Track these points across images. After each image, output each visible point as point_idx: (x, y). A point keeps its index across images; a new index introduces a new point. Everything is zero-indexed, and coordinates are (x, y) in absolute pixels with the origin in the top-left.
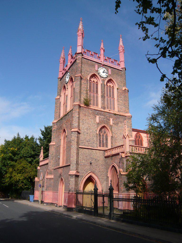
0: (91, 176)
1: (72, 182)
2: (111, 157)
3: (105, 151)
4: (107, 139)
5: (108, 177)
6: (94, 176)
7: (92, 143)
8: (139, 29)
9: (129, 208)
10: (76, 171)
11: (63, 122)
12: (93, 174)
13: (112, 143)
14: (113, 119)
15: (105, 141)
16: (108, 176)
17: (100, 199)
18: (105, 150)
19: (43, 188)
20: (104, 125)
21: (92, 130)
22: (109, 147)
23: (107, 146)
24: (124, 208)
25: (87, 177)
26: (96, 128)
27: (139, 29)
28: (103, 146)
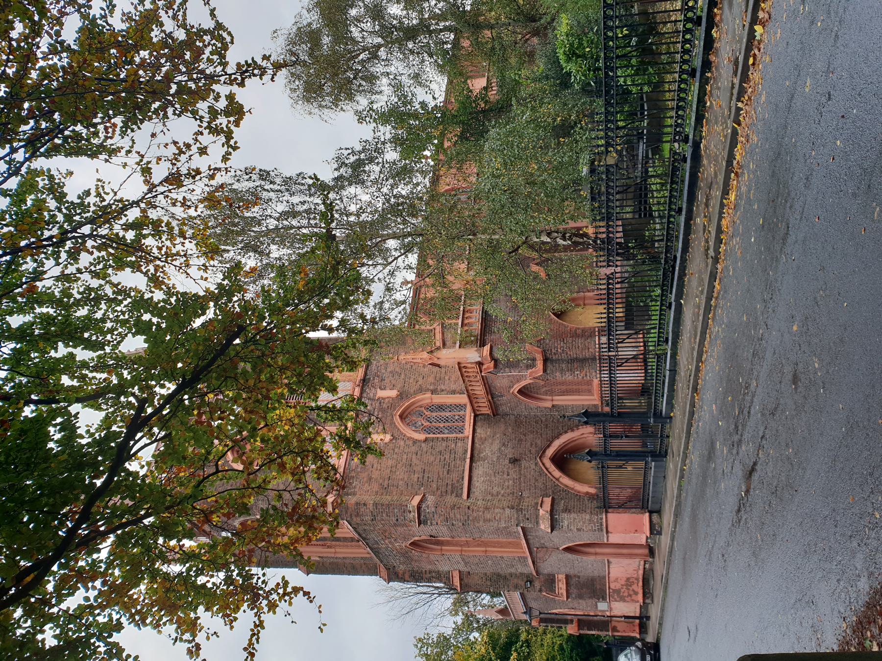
0: (553, 459)
1: (574, 521)
2: (492, 398)
3: (476, 416)
4: (441, 407)
5: (553, 406)
6: (550, 452)
7: (452, 456)
8: (253, 59)
9: (640, 342)
10: (539, 508)
11: (387, 548)
12: (547, 451)
13: (453, 392)
14: (382, 389)
15: (448, 414)
16: (550, 406)
17: (617, 444)
18: (473, 414)
19: (606, 518)
20: (398, 417)
21: (414, 456)
22: (463, 399)
23: (462, 407)
24: (640, 368)
25: (557, 473)
26: (408, 442)
27: (253, 59)
28: (462, 419)
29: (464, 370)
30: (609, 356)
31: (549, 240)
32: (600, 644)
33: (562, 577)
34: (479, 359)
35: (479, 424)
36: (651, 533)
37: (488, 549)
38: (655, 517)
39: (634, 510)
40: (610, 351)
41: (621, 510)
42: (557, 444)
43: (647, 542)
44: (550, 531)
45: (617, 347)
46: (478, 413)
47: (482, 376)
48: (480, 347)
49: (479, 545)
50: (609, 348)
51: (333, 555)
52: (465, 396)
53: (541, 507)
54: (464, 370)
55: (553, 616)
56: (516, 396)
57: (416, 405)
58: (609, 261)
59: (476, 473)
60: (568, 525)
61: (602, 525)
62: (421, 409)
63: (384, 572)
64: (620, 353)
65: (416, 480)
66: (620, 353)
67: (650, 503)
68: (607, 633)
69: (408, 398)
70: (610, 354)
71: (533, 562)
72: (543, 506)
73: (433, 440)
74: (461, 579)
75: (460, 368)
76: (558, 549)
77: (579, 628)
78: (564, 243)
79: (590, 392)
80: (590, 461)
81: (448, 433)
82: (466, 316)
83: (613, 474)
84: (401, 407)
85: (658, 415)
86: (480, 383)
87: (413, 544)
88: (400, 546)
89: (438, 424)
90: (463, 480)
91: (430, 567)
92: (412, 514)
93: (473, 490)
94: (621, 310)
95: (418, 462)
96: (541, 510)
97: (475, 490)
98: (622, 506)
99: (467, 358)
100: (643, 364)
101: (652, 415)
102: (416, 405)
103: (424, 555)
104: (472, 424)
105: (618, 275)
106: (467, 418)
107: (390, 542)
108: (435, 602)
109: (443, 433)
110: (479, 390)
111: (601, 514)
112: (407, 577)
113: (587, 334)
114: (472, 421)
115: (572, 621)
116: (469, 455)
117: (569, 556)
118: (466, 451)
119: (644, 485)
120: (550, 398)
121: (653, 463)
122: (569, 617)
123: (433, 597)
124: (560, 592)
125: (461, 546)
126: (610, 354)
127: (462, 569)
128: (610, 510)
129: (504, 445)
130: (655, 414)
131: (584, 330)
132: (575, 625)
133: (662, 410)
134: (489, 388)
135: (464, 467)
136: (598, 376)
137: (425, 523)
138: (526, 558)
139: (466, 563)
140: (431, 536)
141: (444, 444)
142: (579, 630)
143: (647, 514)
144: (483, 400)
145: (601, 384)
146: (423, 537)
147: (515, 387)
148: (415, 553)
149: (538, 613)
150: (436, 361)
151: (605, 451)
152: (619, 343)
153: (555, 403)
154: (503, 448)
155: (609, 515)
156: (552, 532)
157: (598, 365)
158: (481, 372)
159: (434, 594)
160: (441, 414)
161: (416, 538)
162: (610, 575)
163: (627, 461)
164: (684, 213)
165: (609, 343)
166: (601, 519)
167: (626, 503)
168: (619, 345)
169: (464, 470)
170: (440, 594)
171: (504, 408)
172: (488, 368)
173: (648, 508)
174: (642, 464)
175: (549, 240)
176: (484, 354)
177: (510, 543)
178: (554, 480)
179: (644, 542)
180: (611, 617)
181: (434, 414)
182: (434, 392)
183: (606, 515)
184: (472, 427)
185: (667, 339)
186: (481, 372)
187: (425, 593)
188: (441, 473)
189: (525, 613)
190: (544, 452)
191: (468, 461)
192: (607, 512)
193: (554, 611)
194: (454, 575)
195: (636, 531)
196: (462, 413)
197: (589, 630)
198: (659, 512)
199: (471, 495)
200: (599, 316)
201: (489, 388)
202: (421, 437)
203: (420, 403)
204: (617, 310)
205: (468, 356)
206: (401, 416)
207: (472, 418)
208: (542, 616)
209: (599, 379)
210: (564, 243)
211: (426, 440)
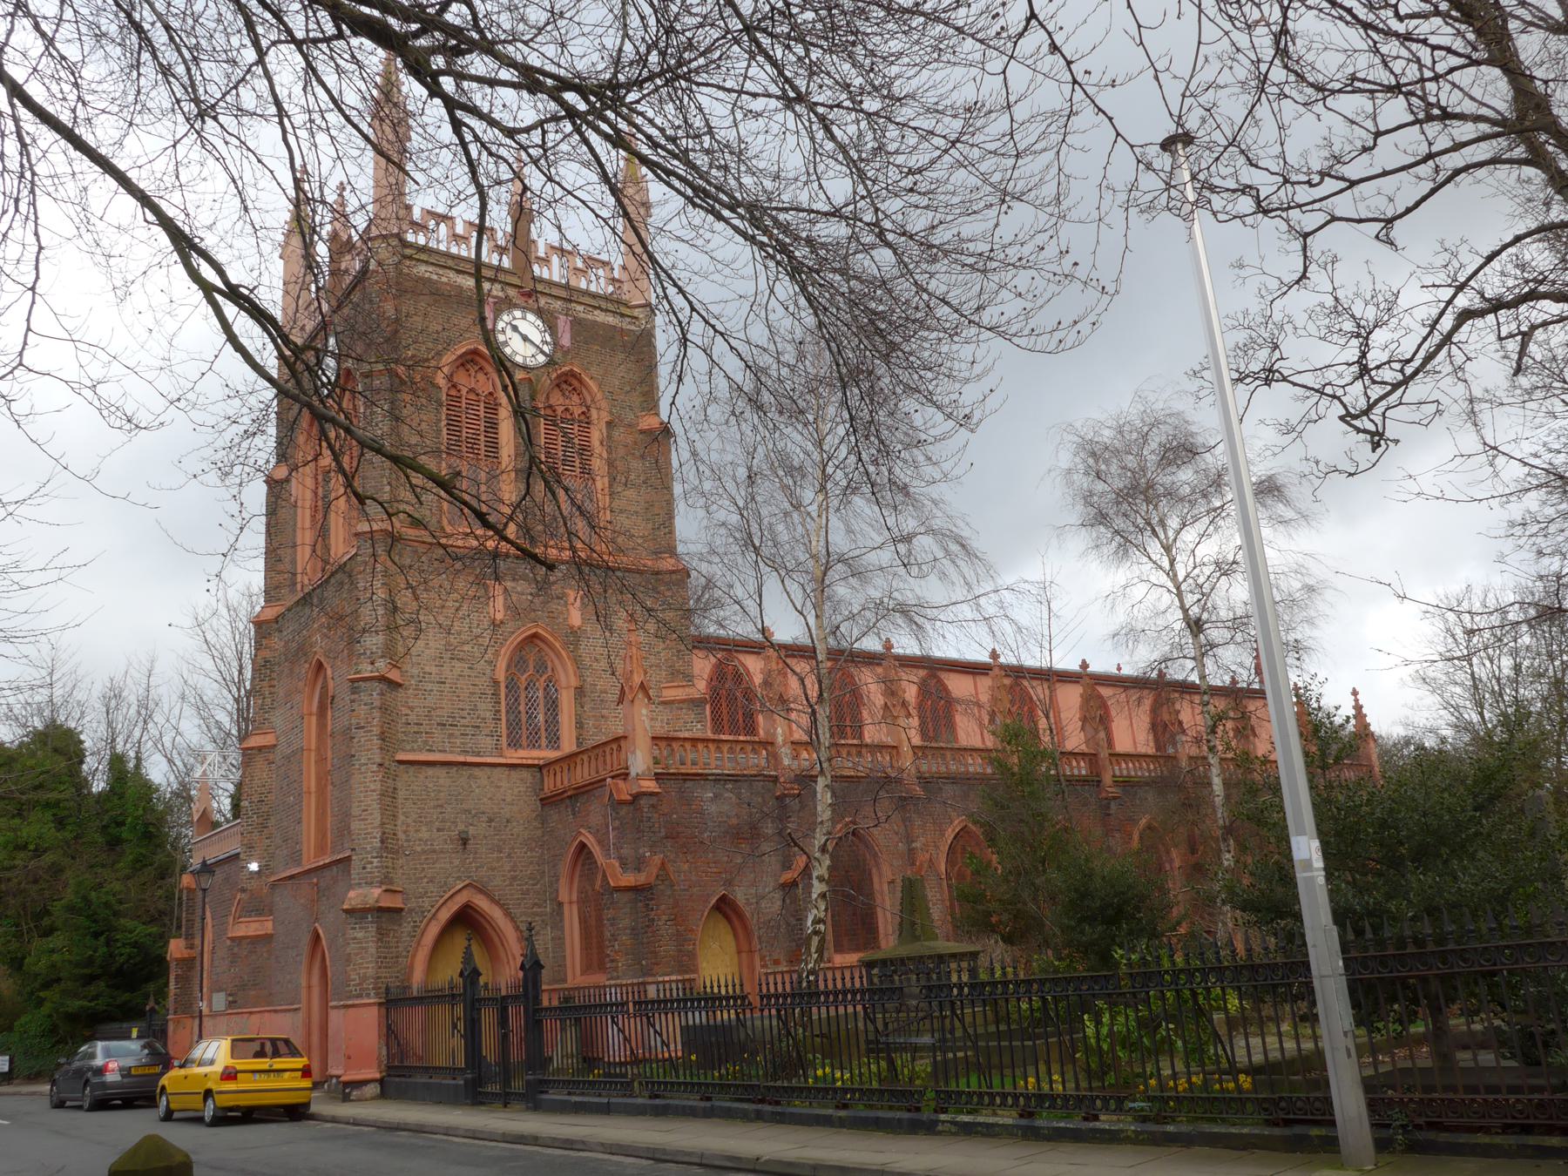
3: (540, 768)
6: (482, 903)
10: (384, 887)
12: (482, 896)
13: (580, 725)
18: (541, 762)
19: (369, 1004)
20: (534, 631)
22: (568, 745)
23: (554, 741)
28: (534, 744)
29: (615, 746)
30: (627, 1003)
31: (814, 896)
32: (152, 998)
33: (268, 927)
34: (633, 773)
35: (525, 774)
36: (347, 1084)
37: (313, 796)
38: (372, 1089)
39: (384, 1052)
40: (635, 1003)
41: (385, 1030)
42: (496, 914)
43: (332, 1077)
44: (345, 907)
45: (641, 1016)
46: (545, 771)
47: (605, 780)
48: (656, 774)
49: (319, 779)
50: (640, 1003)
51: (299, 525)
52: (574, 748)
53: (386, 891)
54: (615, 746)
55: (199, 912)
56: (575, 838)
57: (556, 661)
58: (769, 997)
59: (441, 772)
60: (355, 938)
61: (360, 996)
62: (549, 669)
63: (271, 613)
64: (632, 1020)
65: (427, 669)
66: (632, 1020)
67: (397, 1079)
68: (171, 1012)
69: (566, 644)
70: (631, 1005)
71: (291, 877)
72: (388, 894)
73: (496, 694)
74: (260, 749)
75: (617, 740)
76: (317, 920)
77: (180, 961)
78: (809, 923)
79: (587, 969)
80: (461, 974)
81: (507, 721)
82: (710, 745)
83: (443, 1015)
84: (552, 636)
85: (542, 1085)
86: (594, 776)
87: (320, 666)
88: (316, 642)
89: (522, 700)
90: (429, 750)
91: (281, 694)
92: (370, 668)
93: (412, 769)
94: (697, 1021)
95: (457, 671)
96: (379, 890)
97: (411, 773)
98: (390, 1033)
99: (634, 752)
100: (648, 1066)
101: (540, 1077)
102: (556, 661)
103: (301, 684)
104: (524, 762)
105: (748, 1015)
106: (536, 753)
107: (322, 626)
108: (225, 692)
109: (507, 712)
110: (583, 774)
111: (377, 994)
112: (263, 654)
113: (686, 962)
114: (530, 762)
115: (191, 947)
116: (470, 759)
117: (306, 940)
118: (478, 754)
119: (427, 1069)
120: (575, 897)
121: (462, 1082)
122: (197, 941)
123: (234, 690)
124: (243, 925)
125: (318, 749)
126: (631, 1005)
127: (278, 750)
128: (383, 1011)
129: (491, 820)
130: (541, 1082)
131: (692, 956)
132: (186, 953)
133: (547, 1092)
134: (583, 793)
135: (451, 752)
136: (613, 982)
137: (354, 691)
138: (299, 864)
139: (288, 758)
140: (333, 698)
141: (488, 715)
142: (177, 960)
143: (378, 1076)
144: (566, 782)
145: (599, 987)
146: (331, 684)
147: (590, 836)
148: (304, 669)
149: (203, 886)
150: (629, 696)
151: (479, 1000)
152: (648, 1018)
153: (566, 908)
154: (484, 818)
155: (375, 1009)
156: (344, 911)
157: (635, 981)
158: (613, 777)
159: (239, 690)
160: (542, 706)
161: (329, 672)
162: (274, 1015)
163: (464, 1037)
164: (703, 1104)
165: (647, 1003)
166: (368, 996)
167: (396, 1037)
168: (644, 1019)
169: (445, 751)
170: (237, 701)
171: (555, 817)
172: (618, 790)
173: (389, 1075)
174: (461, 1062)
175: (814, 896)
176: (643, 783)
177: (324, 835)
178: (433, 910)
179: (333, 1071)
180: (201, 1017)
181: (541, 694)
182: (580, 692)
183: (374, 1004)
184: (519, 761)
185: (657, 1097)
186: (613, 777)
187: (240, 673)
188: (439, 712)
189: (204, 862)
190: (481, 891)
191: (461, 759)
192: (380, 1004)
193: (208, 914)
194: (268, 736)
195: (349, 1058)
196: (544, 742)
197: (177, 976)
198: (384, 1094)
199: (402, 767)
200: (723, 983)
201: (583, 793)
202: (501, 675)
203: (559, 667)
204: (823, 1010)
205: (638, 753)
206: (535, 636)
207: (536, 762)
208: (200, 894)
209: (607, 983)
210: (809, 923)
211: (496, 683)
